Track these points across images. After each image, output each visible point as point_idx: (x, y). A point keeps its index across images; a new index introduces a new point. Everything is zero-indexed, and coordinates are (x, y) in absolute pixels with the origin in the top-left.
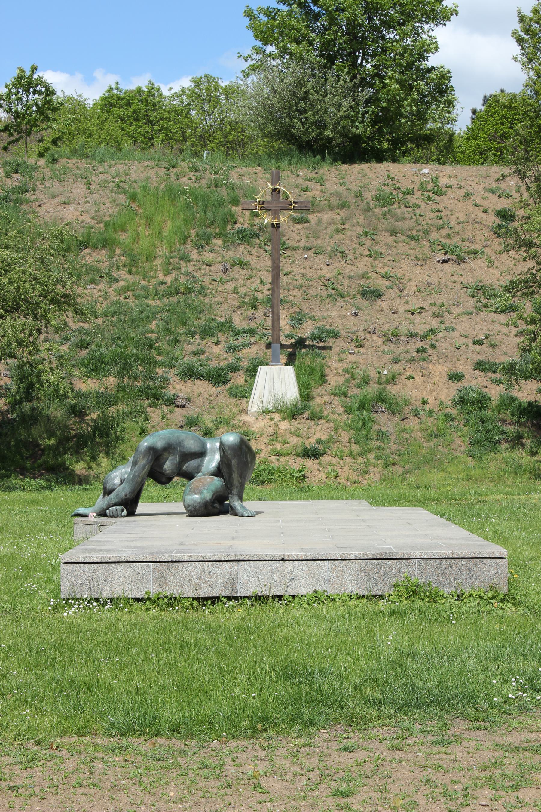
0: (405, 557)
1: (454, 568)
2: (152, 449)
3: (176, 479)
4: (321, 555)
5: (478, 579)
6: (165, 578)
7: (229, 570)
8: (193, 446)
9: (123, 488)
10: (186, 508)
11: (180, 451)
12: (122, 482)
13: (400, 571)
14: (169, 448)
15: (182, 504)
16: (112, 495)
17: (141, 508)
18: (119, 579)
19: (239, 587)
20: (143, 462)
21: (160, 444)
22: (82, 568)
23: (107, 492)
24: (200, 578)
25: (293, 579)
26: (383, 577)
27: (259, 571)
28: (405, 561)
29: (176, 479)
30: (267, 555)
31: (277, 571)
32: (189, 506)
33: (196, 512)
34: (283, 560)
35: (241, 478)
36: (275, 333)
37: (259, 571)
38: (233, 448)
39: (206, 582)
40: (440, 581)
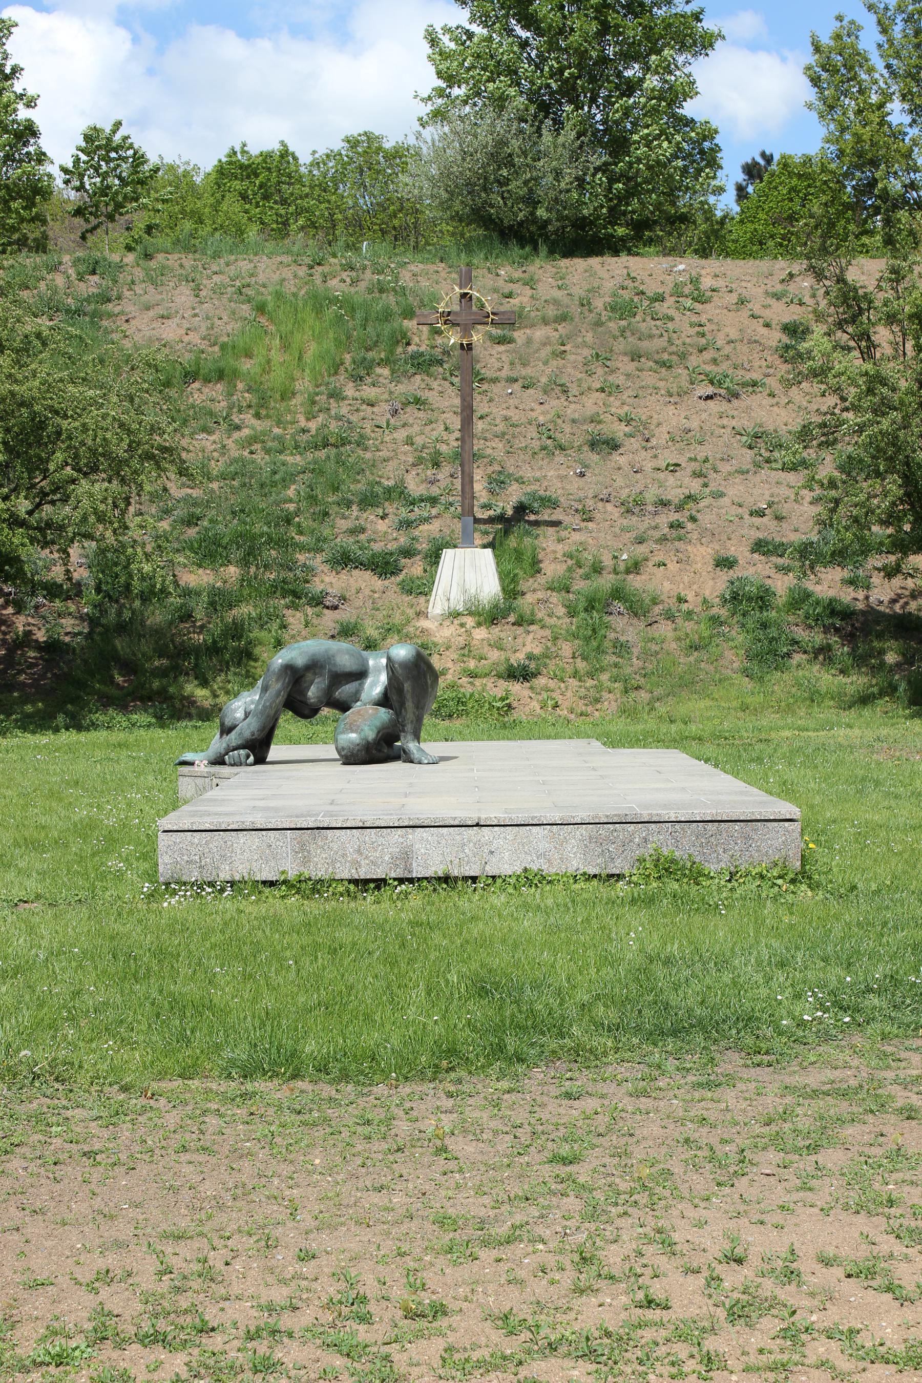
2: (289, 668)
4: (533, 818)
6: (309, 852)
7: (401, 840)
8: (348, 664)
10: (339, 753)
11: (330, 671)
14: (314, 666)
16: (233, 735)
17: (275, 752)
18: (242, 854)
19: (414, 865)
21: (300, 662)
22: (189, 839)
25: (492, 852)
26: (622, 849)
28: (653, 825)
32: (343, 749)
34: (477, 825)
35: (417, 708)
36: (467, 502)
37: (444, 842)
38: (405, 665)
40: (704, 854)
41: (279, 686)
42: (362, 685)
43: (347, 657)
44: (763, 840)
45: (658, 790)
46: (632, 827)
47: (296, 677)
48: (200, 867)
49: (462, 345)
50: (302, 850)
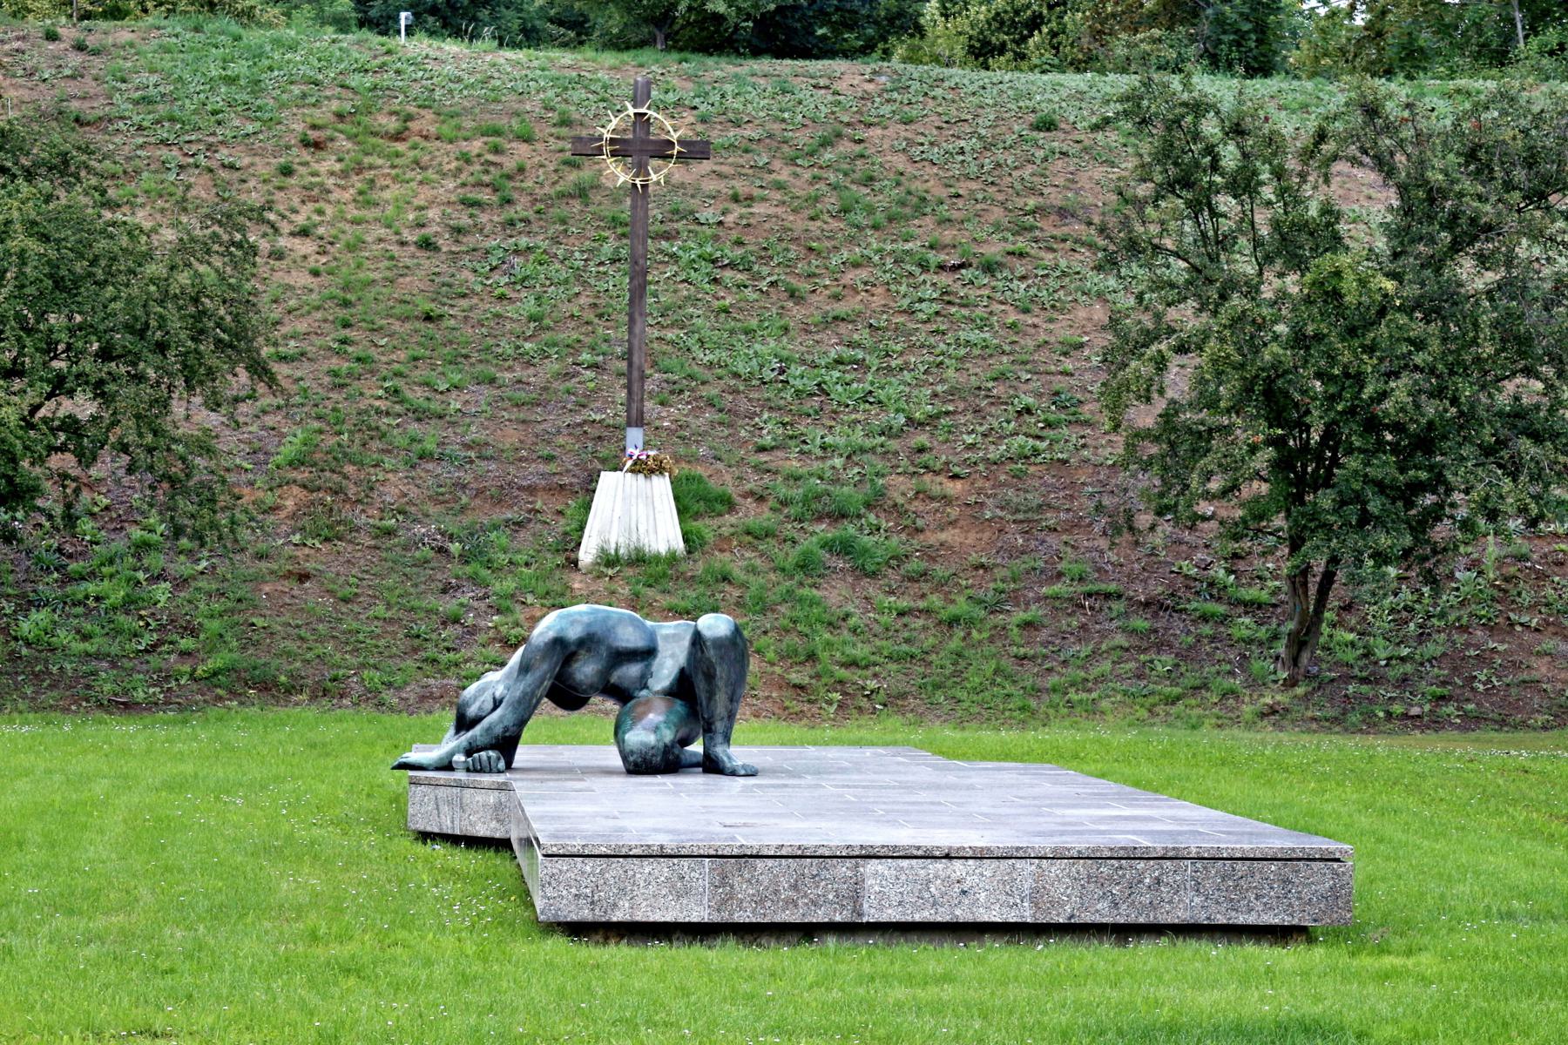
0: (1170, 854)
1: (1258, 876)
2: (558, 643)
3: (596, 699)
4: (1018, 849)
5: (1299, 899)
6: (732, 887)
7: (849, 873)
8: (632, 638)
9: (501, 719)
10: (624, 758)
11: (609, 648)
12: (497, 704)
13: (1158, 881)
14: (589, 642)
15: (614, 750)
16: (477, 730)
17: (522, 755)
18: (646, 887)
19: (866, 906)
20: (543, 668)
21: (574, 633)
22: (579, 866)
23: (464, 723)
24: (795, 887)
25: (964, 892)
26: (1128, 892)
27: (903, 877)
28: (1168, 863)
29: (596, 699)
30: (918, 848)
31: (936, 877)
32: (632, 752)
33: (640, 765)
34: (947, 857)
35: (731, 700)
36: (634, 406)
37: (903, 877)
38: (719, 643)
39: (806, 895)
40: (1232, 900)
41: (545, 667)
42: (648, 666)
43: (631, 629)
44: (1305, 885)
45: (1126, 818)
46: (1141, 865)
47: (564, 651)
48: (592, 903)
49: (634, 185)
50: (723, 885)
